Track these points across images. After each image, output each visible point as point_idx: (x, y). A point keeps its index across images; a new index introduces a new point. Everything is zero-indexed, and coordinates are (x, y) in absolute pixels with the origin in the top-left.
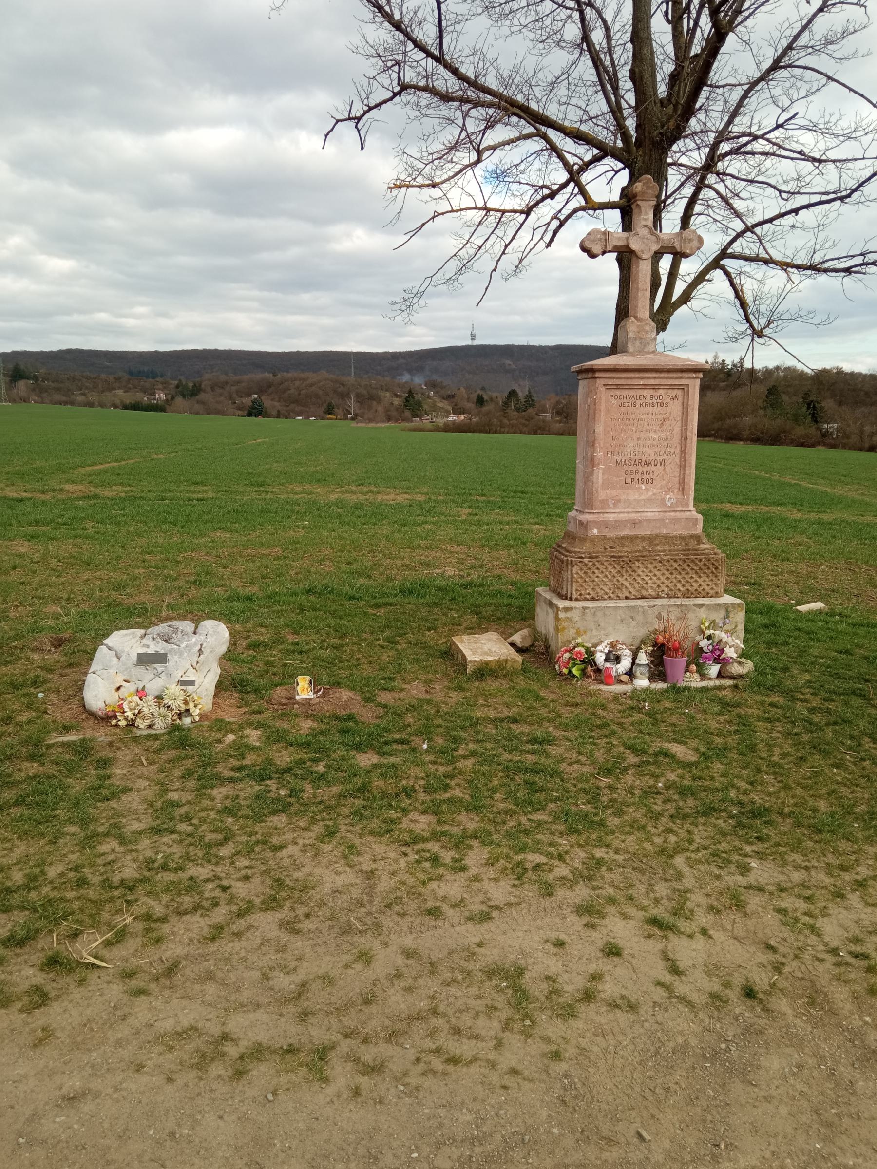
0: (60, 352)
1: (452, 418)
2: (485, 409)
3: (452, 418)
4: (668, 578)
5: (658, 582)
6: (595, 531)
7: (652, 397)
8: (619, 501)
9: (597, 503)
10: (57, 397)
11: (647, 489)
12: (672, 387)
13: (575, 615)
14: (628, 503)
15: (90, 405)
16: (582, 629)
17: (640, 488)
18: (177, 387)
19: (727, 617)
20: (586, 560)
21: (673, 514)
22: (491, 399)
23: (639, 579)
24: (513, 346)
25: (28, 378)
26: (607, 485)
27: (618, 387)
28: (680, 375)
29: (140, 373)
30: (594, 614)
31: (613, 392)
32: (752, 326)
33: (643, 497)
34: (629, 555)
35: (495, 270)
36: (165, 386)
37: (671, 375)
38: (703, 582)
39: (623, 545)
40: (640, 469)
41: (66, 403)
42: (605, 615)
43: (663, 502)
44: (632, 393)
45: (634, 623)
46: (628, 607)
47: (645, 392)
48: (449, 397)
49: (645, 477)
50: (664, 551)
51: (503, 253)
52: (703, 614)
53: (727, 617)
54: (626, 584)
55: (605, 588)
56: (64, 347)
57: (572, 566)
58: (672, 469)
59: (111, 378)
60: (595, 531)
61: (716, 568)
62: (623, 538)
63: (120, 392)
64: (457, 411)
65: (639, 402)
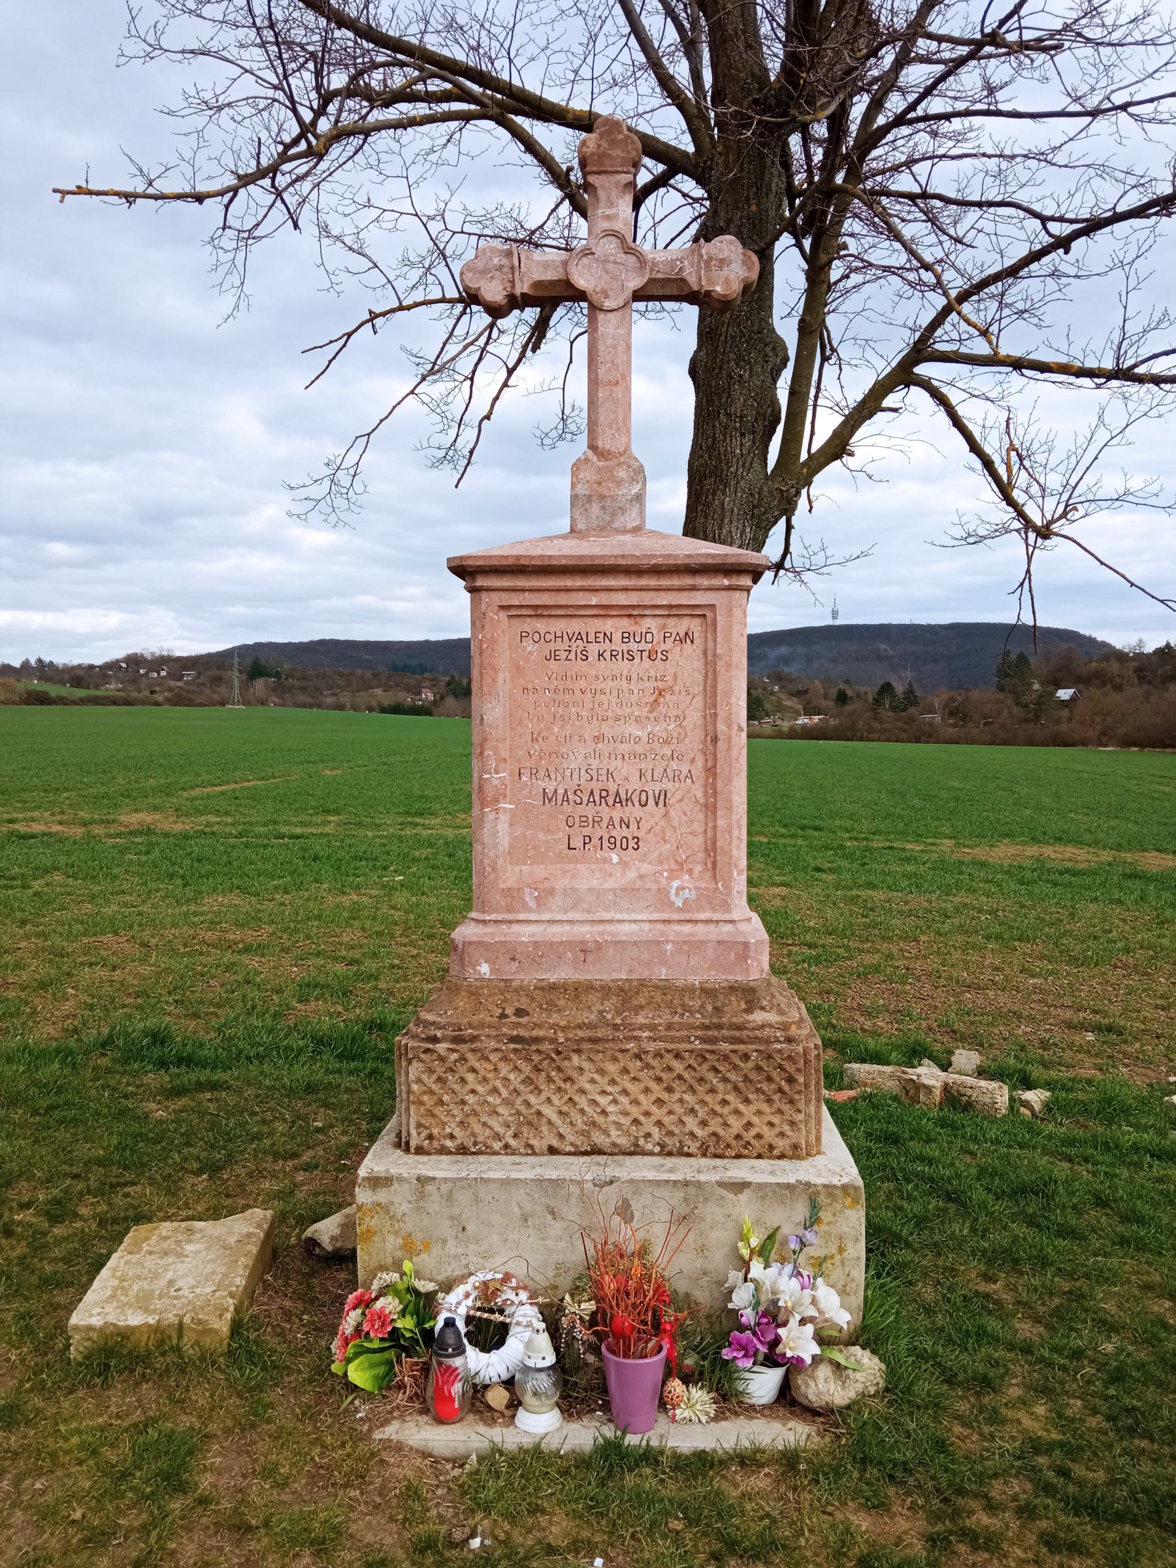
0: (312, 642)
1: (803, 720)
2: (848, 708)
3: (803, 720)
4: (659, 1102)
5: (635, 1111)
6: (485, 969)
7: (626, 637)
8: (551, 892)
9: (496, 898)
10: (301, 698)
11: (624, 864)
12: (673, 611)
13: (400, 1198)
14: (575, 899)
15: (341, 707)
16: (418, 1236)
17: (607, 860)
18: (449, 684)
19: (812, 1221)
20: (441, 1047)
21: (687, 928)
22: (858, 695)
23: (583, 1102)
24: (890, 626)
25: (270, 676)
26: (520, 852)
27: (538, 612)
28: (688, 581)
29: (406, 668)
30: (450, 1197)
31: (529, 625)
32: (1021, 514)
33: (611, 883)
34: (561, 1032)
35: (488, 417)
36: (434, 682)
37: (665, 582)
38: (757, 1115)
39: (552, 1007)
40: (605, 812)
41: (311, 706)
42: (477, 1200)
43: (662, 899)
44: (575, 626)
45: (557, 1227)
46: (539, 1182)
47: (608, 625)
48: (800, 694)
49: (618, 833)
50: (652, 1027)
51: (505, 385)
52: (744, 1208)
53: (812, 1221)
54: (549, 1112)
55: (494, 1123)
56: (316, 638)
57: (410, 1062)
58: (685, 814)
59: (368, 674)
60: (485, 969)
61: (791, 1080)
62: (554, 987)
63: (379, 692)
64: (809, 712)
65: (593, 649)
